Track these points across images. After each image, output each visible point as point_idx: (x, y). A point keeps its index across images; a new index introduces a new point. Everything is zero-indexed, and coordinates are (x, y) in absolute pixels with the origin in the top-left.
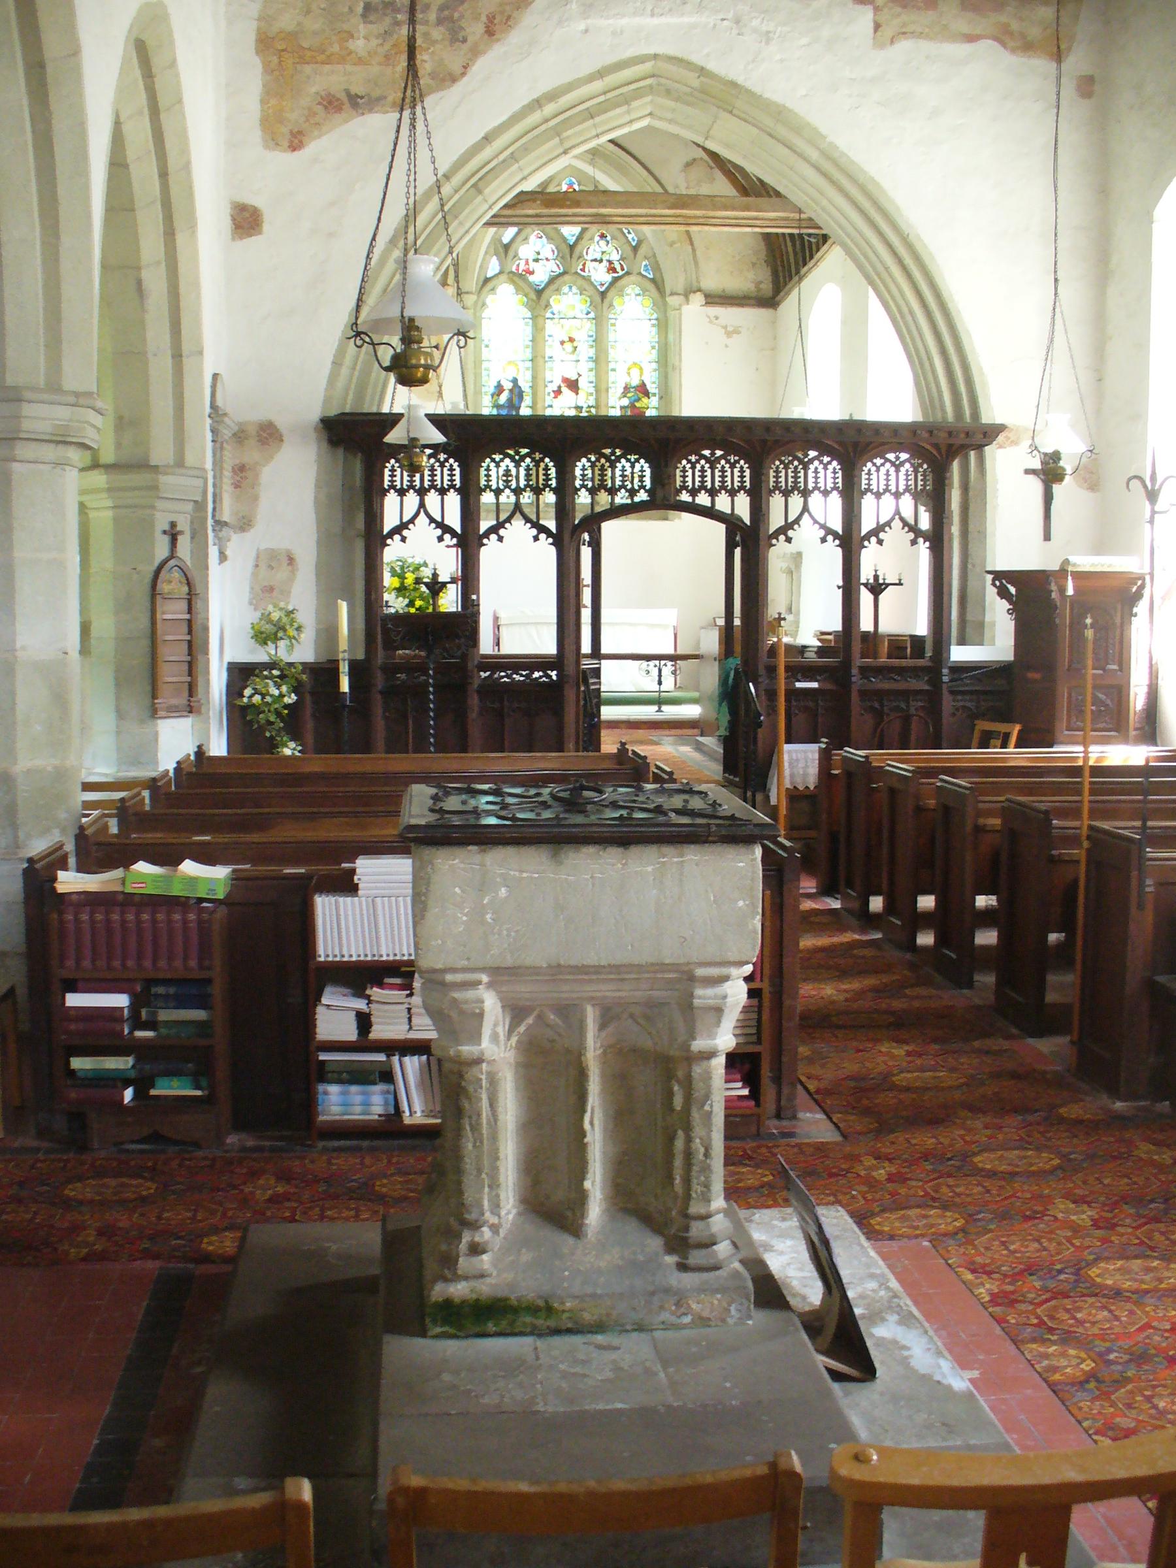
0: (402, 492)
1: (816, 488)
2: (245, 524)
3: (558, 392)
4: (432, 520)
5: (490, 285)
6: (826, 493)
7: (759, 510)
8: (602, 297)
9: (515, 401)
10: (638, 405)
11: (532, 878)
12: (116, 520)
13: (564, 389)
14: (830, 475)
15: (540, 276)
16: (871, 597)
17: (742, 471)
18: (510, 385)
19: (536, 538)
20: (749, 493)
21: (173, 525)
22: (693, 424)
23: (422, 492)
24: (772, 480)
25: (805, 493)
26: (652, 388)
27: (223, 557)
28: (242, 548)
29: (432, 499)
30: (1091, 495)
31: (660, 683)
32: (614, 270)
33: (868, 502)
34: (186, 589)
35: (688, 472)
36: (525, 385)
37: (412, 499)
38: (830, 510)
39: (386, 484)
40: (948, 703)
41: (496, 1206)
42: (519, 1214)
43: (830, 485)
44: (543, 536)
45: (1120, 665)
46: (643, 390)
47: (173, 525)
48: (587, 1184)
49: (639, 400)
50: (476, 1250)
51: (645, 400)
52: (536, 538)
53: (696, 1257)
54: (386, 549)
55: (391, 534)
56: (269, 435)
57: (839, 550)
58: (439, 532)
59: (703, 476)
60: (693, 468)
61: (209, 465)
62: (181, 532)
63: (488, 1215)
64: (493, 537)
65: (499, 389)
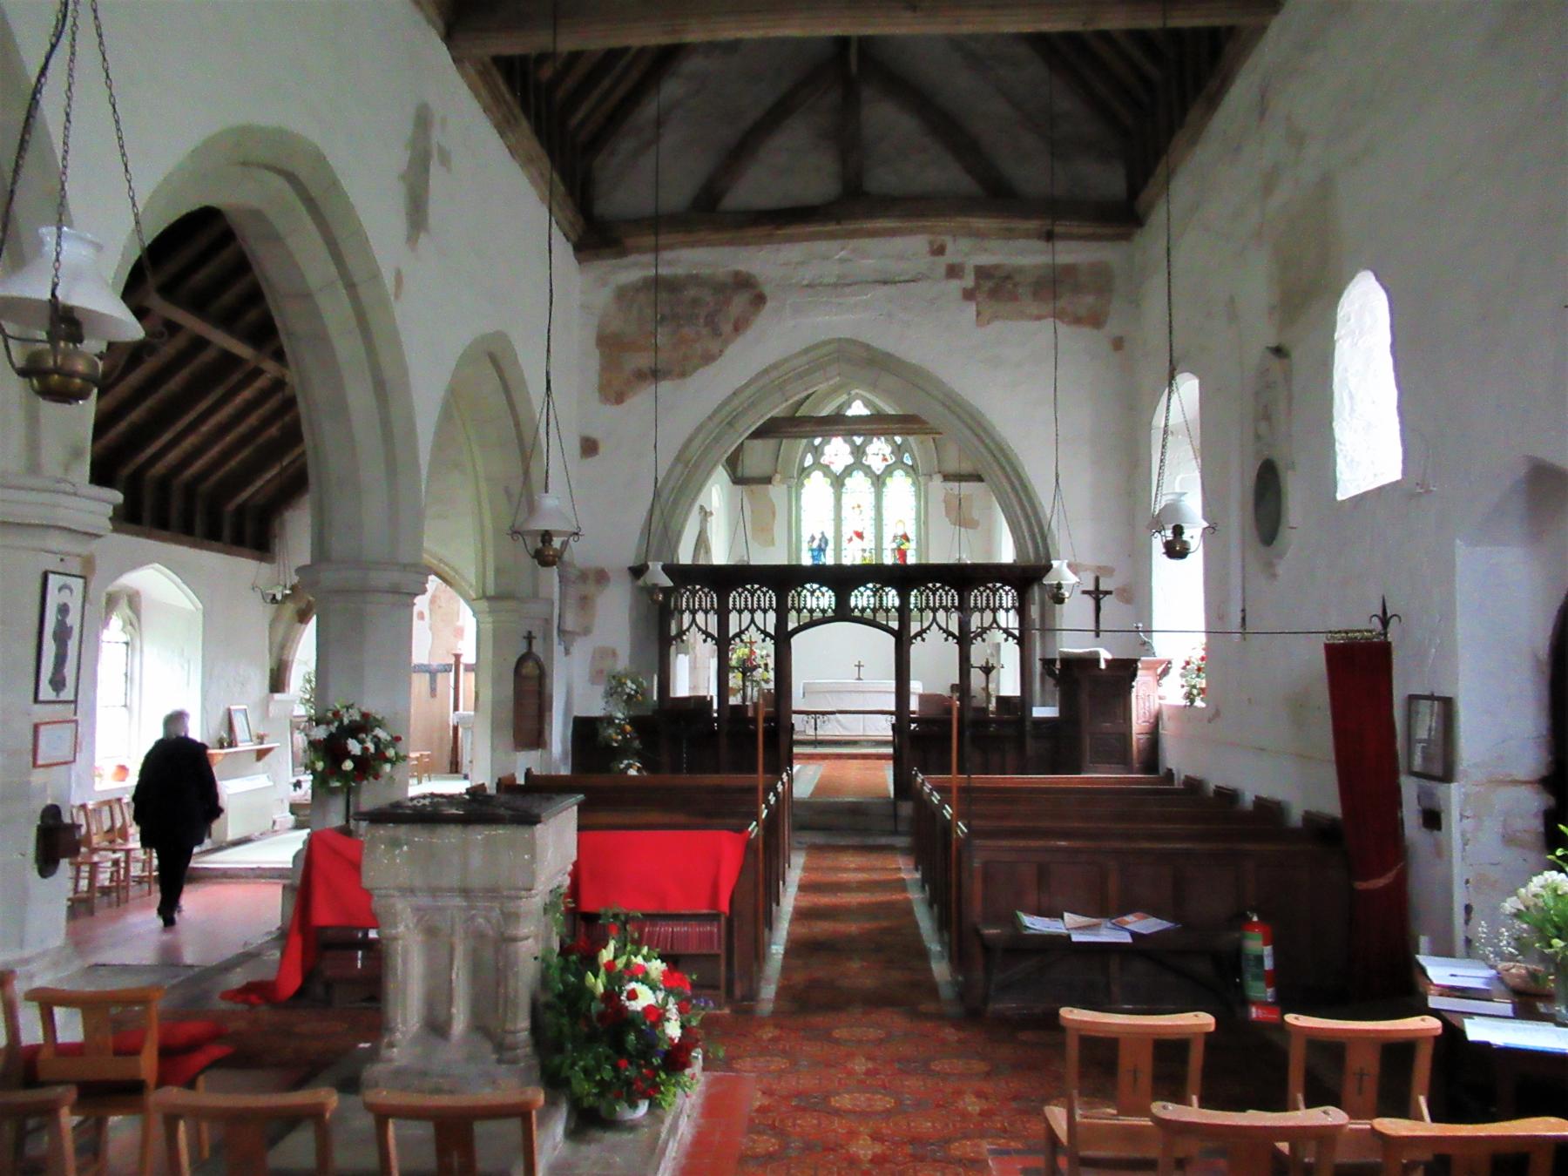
0: (740, 612)
1: (793, 608)
2: (586, 631)
3: (851, 540)
4: (940, 628)
5: (806, 473)
6: (1007, 610)
7: (723, 624)
8: (878, 481)
9: (823, 546)
10: (902, 547)
11: (1514, 893)
12: (494, 630)
13: (855, 538)
14: (1010, 598)
15: (837, 468)
16: (983, 676)
17: (953, 596)
18: (820, 536)
19: (946, 640)
20: (716, 612)
21: (530, 633)
22: (854, 569)
23: (752, 611)
24: (972, 602)
25: (994, 611)
26: (912, 536)
27: (567, 652)
28: (582, 650)
29: (759, 616)
30: (1129, 606)
31: (816, 729)
32: (885, 460)
33: (733, 617)
34: (538, 672)
35: (861, 598)
36: (830, 536)
37: (746, 616)
38: (1009, 620)
39: (731, 606)
40: (1029, 743)
41: (405, 1022)
42: (421, 1027)
43: (1010, 605)
44: (1010, 639)
45: (1125, 720)
46: (906, 538)
47: (530, 633)
48: (454, 1010)
49: (903, 544)
50: (391, 1045)
51: (907, 544)
52: (946, 640)
53: (508, 1055)
54: (913, 646)
55: (915, 637)
56: (601, 577)
57: (957, 646)
58: (945, 635)
59: (746, 601)
60: (981, 595)
61: (556, 596)
62: (535, 638)
63: (400, 1026)
64: (919, 638)
65: (813, 539)
